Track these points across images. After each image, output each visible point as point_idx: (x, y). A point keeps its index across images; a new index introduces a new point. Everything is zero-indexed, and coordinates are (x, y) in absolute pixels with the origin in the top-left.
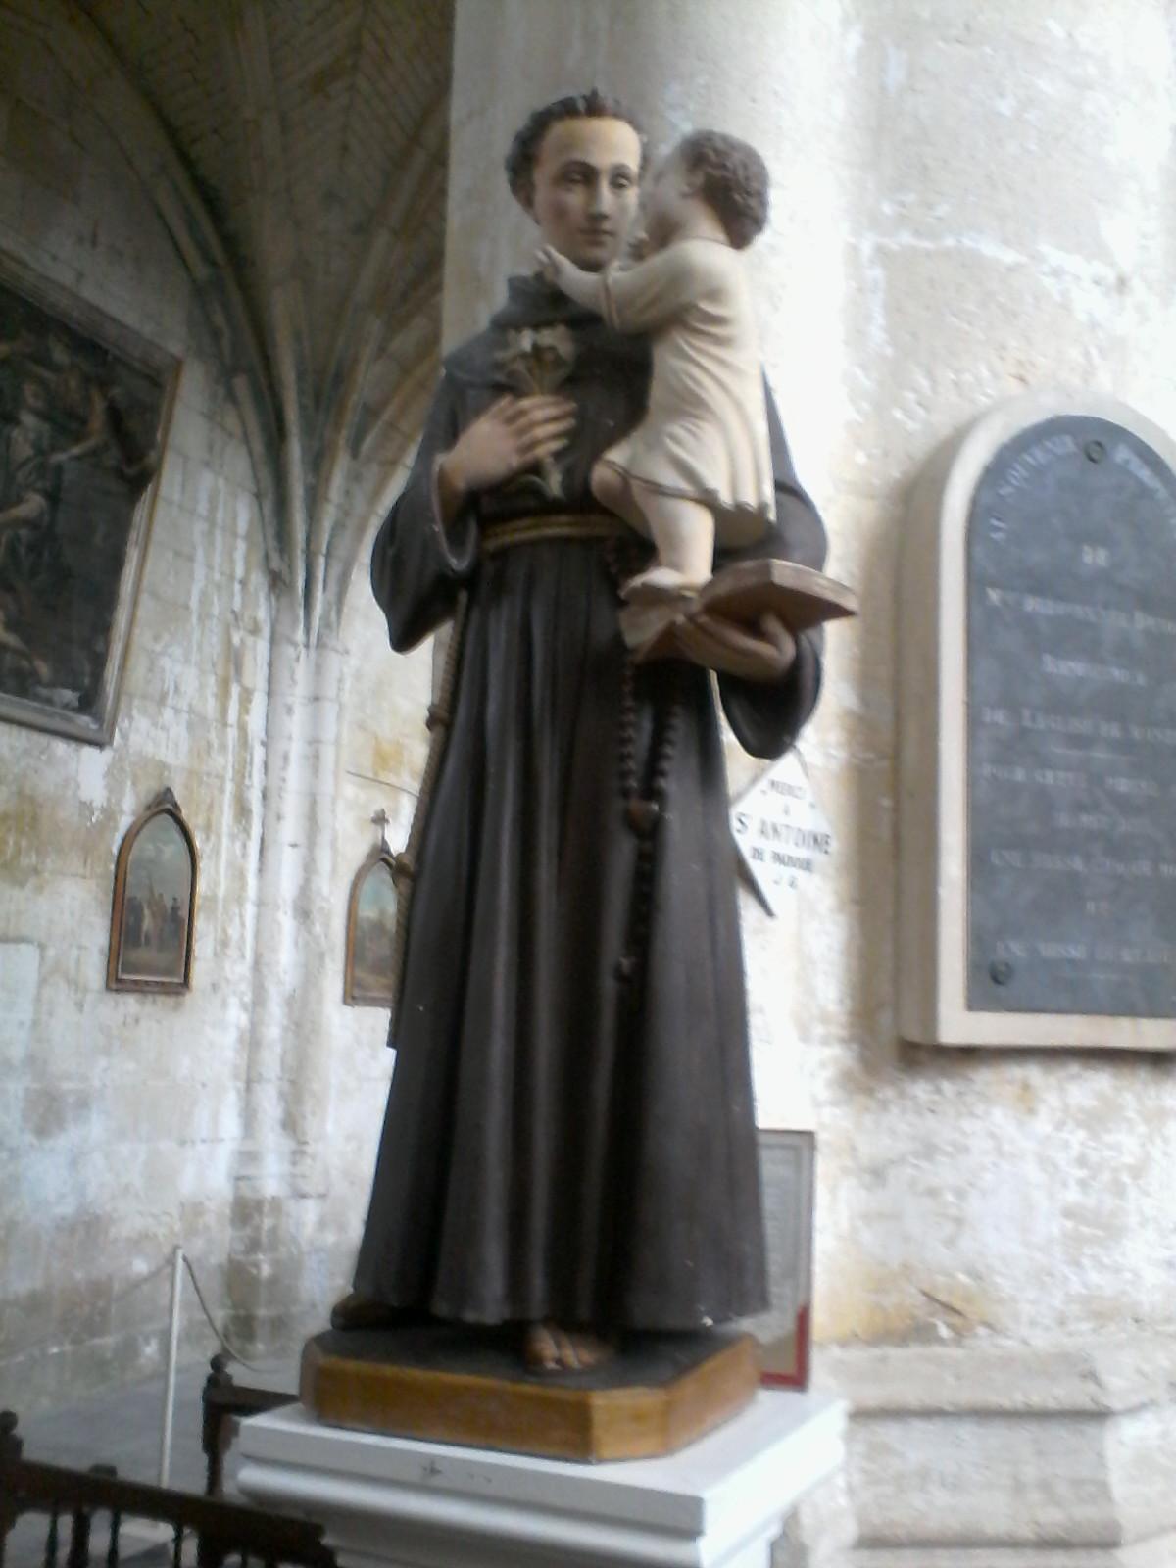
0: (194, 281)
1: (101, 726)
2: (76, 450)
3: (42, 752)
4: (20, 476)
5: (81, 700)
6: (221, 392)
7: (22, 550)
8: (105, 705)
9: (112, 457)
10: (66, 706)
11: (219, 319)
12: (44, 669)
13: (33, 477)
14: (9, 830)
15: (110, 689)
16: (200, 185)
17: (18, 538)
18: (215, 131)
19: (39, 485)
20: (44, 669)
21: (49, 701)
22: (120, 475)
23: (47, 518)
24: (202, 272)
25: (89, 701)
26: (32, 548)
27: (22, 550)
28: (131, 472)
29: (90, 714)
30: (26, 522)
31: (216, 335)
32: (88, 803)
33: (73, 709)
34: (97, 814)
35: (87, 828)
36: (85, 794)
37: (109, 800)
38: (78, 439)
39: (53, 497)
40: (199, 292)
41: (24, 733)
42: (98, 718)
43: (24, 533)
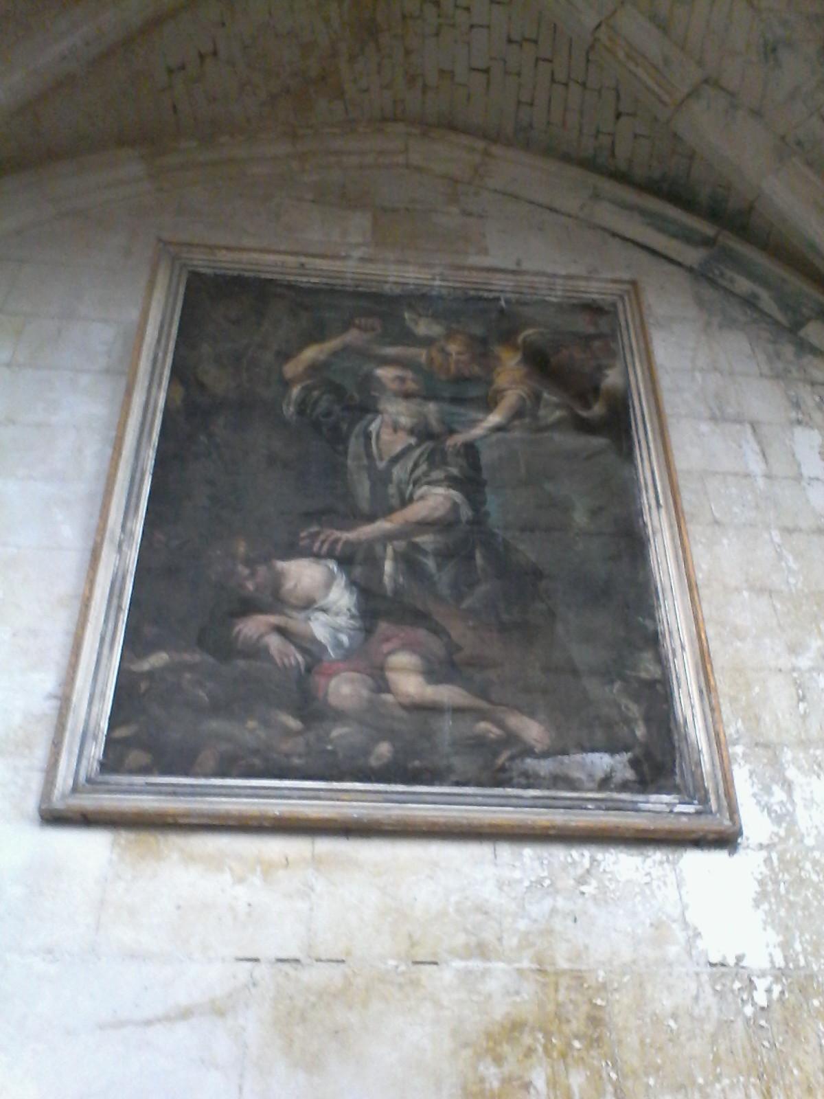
0: (690, 270)
1: (705, 800)
2: (494, 419)
3: (582, 881)
4: (398, 472)
5: (634, 764)
6: (788, 350)
7: (430, 563)
8: (699, 764)
9: (553, 408)
10: (605, 783)
11: (744, 285)
12: (533, 731)
13: (423, 467)
14: (530, 1052)
15: (697, 733)
16: (651, 187)
17: (416, 547)
18: (618, 116)
19: (437, 474)
20: (533, 731)
21: (561, 781)
22: (585, 427)
23: (466, 513)
24: (693, 256)
25: (658, 760)
26: (444, 556)
27: (430, 563)
28: (598, 410)
29: (673, 789)
30: (424, 525)
31: (749, 302)
32: (731, 961)
33: (624, 786)
34: (761, 984)
35: (747, 1020)
36: (716, 947)
37: (786, 946)
38: (489, 404)
39: (471, 482)
40: (700, 275)
41: (528, 852)
42: (696, 793)
43: (426, 540)
